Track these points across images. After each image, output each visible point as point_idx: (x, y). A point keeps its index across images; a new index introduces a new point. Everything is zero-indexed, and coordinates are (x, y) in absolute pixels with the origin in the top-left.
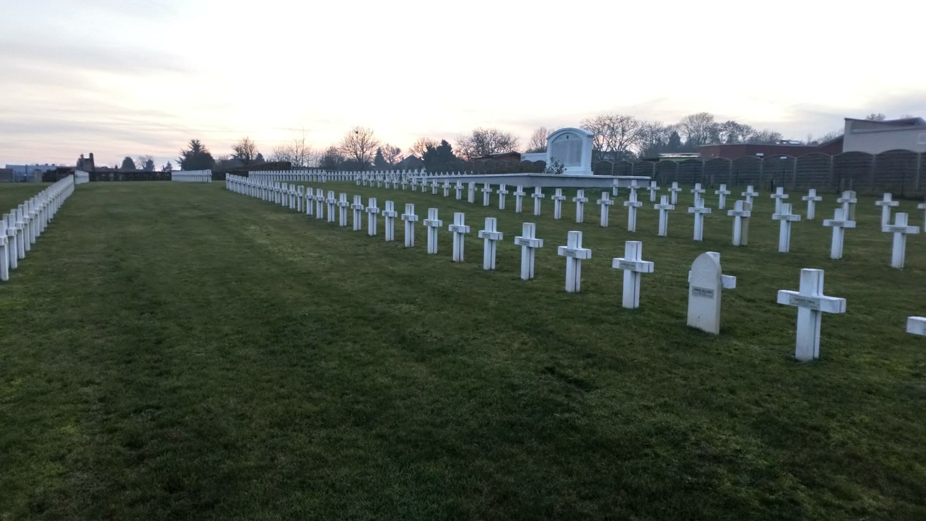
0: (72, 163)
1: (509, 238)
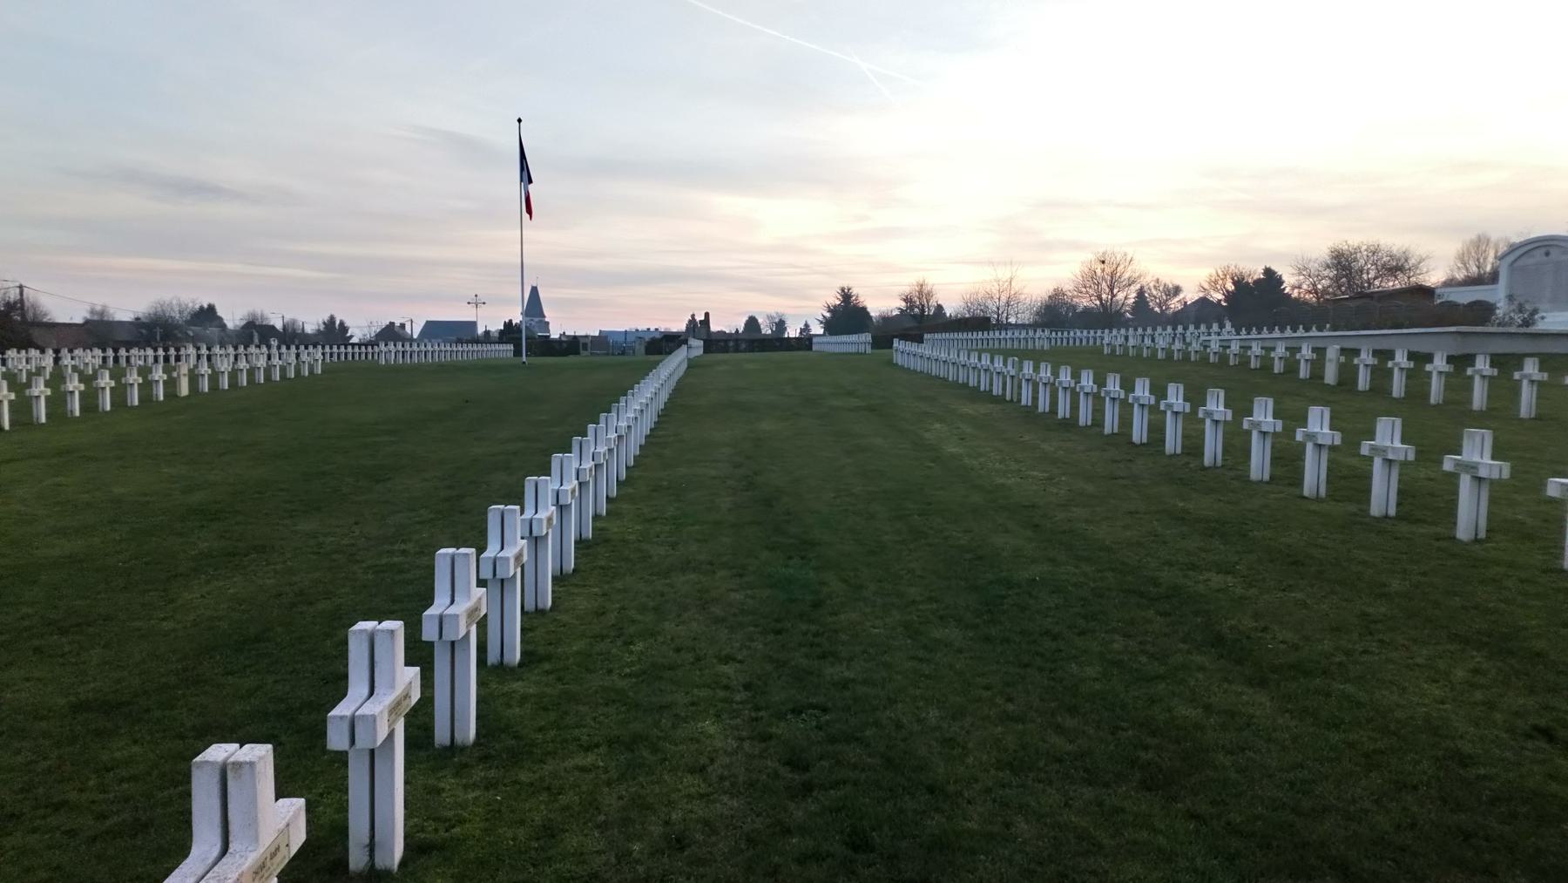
0: (679, 326)
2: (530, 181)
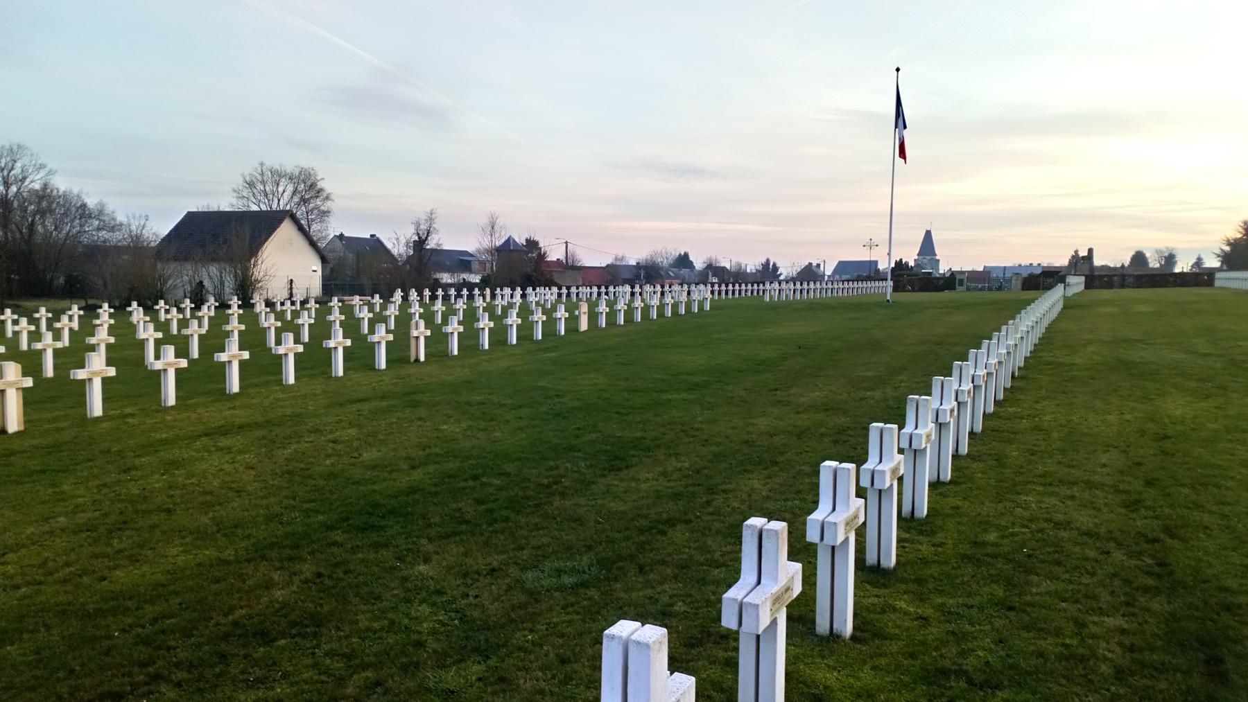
0: (1062, 261)
2: (905, 127)
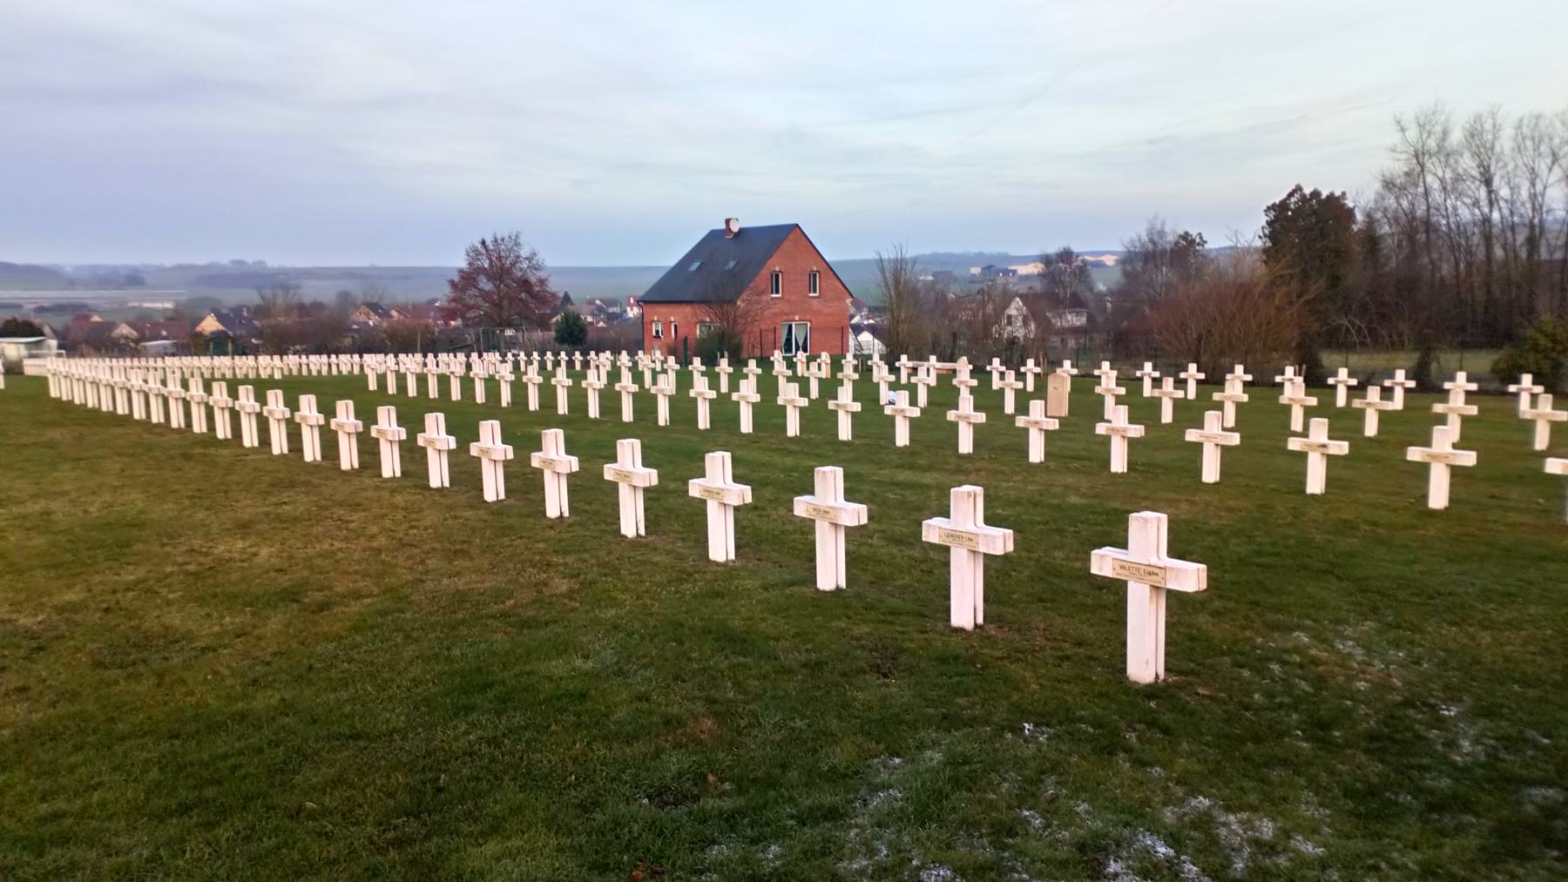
1: (463, 446)
